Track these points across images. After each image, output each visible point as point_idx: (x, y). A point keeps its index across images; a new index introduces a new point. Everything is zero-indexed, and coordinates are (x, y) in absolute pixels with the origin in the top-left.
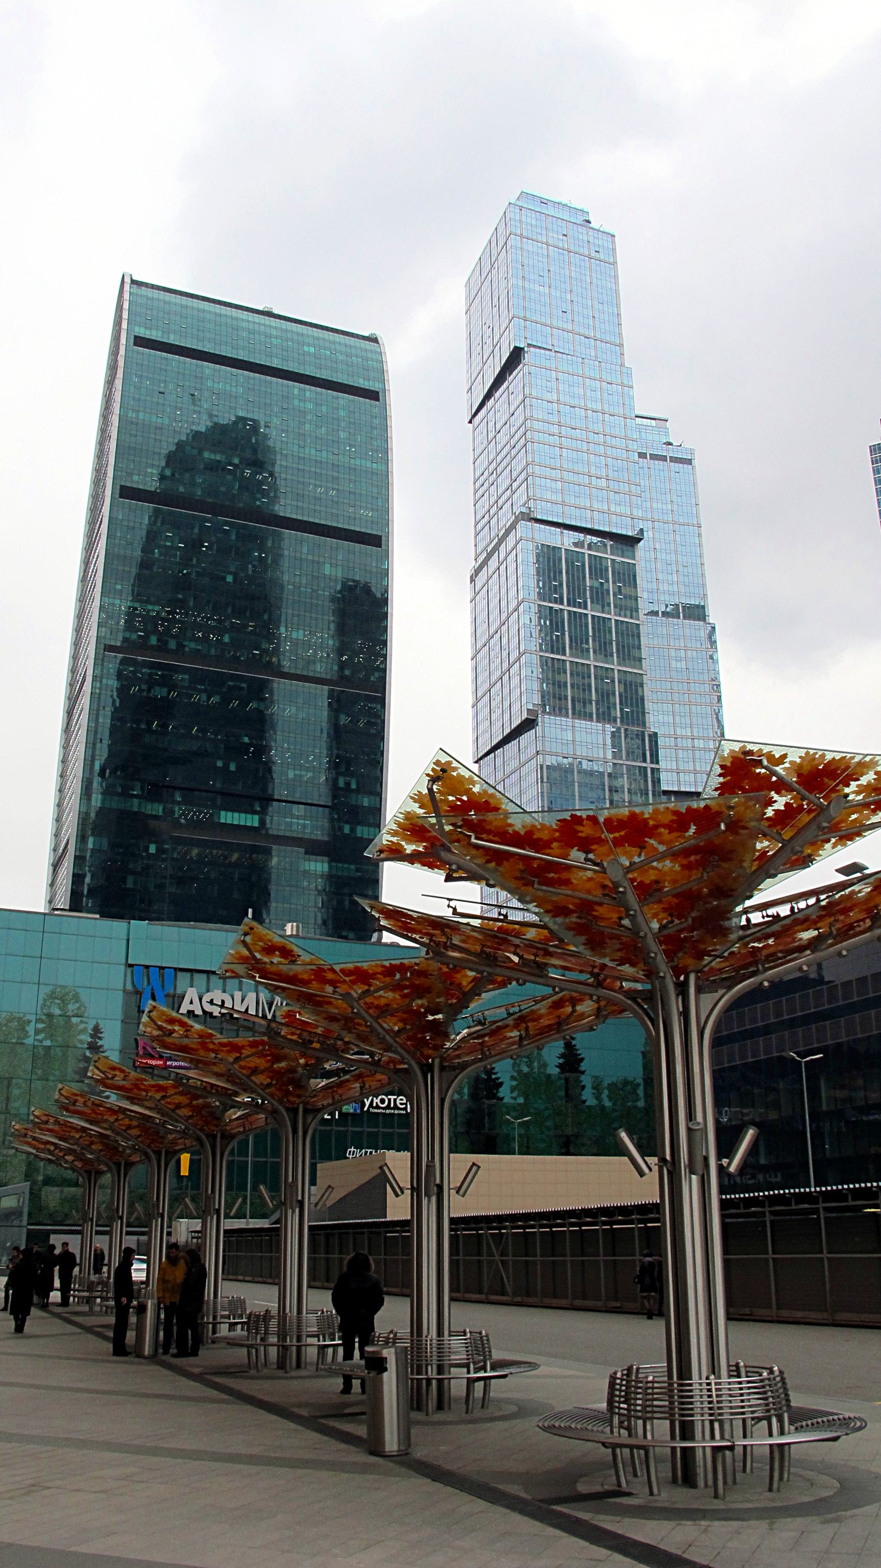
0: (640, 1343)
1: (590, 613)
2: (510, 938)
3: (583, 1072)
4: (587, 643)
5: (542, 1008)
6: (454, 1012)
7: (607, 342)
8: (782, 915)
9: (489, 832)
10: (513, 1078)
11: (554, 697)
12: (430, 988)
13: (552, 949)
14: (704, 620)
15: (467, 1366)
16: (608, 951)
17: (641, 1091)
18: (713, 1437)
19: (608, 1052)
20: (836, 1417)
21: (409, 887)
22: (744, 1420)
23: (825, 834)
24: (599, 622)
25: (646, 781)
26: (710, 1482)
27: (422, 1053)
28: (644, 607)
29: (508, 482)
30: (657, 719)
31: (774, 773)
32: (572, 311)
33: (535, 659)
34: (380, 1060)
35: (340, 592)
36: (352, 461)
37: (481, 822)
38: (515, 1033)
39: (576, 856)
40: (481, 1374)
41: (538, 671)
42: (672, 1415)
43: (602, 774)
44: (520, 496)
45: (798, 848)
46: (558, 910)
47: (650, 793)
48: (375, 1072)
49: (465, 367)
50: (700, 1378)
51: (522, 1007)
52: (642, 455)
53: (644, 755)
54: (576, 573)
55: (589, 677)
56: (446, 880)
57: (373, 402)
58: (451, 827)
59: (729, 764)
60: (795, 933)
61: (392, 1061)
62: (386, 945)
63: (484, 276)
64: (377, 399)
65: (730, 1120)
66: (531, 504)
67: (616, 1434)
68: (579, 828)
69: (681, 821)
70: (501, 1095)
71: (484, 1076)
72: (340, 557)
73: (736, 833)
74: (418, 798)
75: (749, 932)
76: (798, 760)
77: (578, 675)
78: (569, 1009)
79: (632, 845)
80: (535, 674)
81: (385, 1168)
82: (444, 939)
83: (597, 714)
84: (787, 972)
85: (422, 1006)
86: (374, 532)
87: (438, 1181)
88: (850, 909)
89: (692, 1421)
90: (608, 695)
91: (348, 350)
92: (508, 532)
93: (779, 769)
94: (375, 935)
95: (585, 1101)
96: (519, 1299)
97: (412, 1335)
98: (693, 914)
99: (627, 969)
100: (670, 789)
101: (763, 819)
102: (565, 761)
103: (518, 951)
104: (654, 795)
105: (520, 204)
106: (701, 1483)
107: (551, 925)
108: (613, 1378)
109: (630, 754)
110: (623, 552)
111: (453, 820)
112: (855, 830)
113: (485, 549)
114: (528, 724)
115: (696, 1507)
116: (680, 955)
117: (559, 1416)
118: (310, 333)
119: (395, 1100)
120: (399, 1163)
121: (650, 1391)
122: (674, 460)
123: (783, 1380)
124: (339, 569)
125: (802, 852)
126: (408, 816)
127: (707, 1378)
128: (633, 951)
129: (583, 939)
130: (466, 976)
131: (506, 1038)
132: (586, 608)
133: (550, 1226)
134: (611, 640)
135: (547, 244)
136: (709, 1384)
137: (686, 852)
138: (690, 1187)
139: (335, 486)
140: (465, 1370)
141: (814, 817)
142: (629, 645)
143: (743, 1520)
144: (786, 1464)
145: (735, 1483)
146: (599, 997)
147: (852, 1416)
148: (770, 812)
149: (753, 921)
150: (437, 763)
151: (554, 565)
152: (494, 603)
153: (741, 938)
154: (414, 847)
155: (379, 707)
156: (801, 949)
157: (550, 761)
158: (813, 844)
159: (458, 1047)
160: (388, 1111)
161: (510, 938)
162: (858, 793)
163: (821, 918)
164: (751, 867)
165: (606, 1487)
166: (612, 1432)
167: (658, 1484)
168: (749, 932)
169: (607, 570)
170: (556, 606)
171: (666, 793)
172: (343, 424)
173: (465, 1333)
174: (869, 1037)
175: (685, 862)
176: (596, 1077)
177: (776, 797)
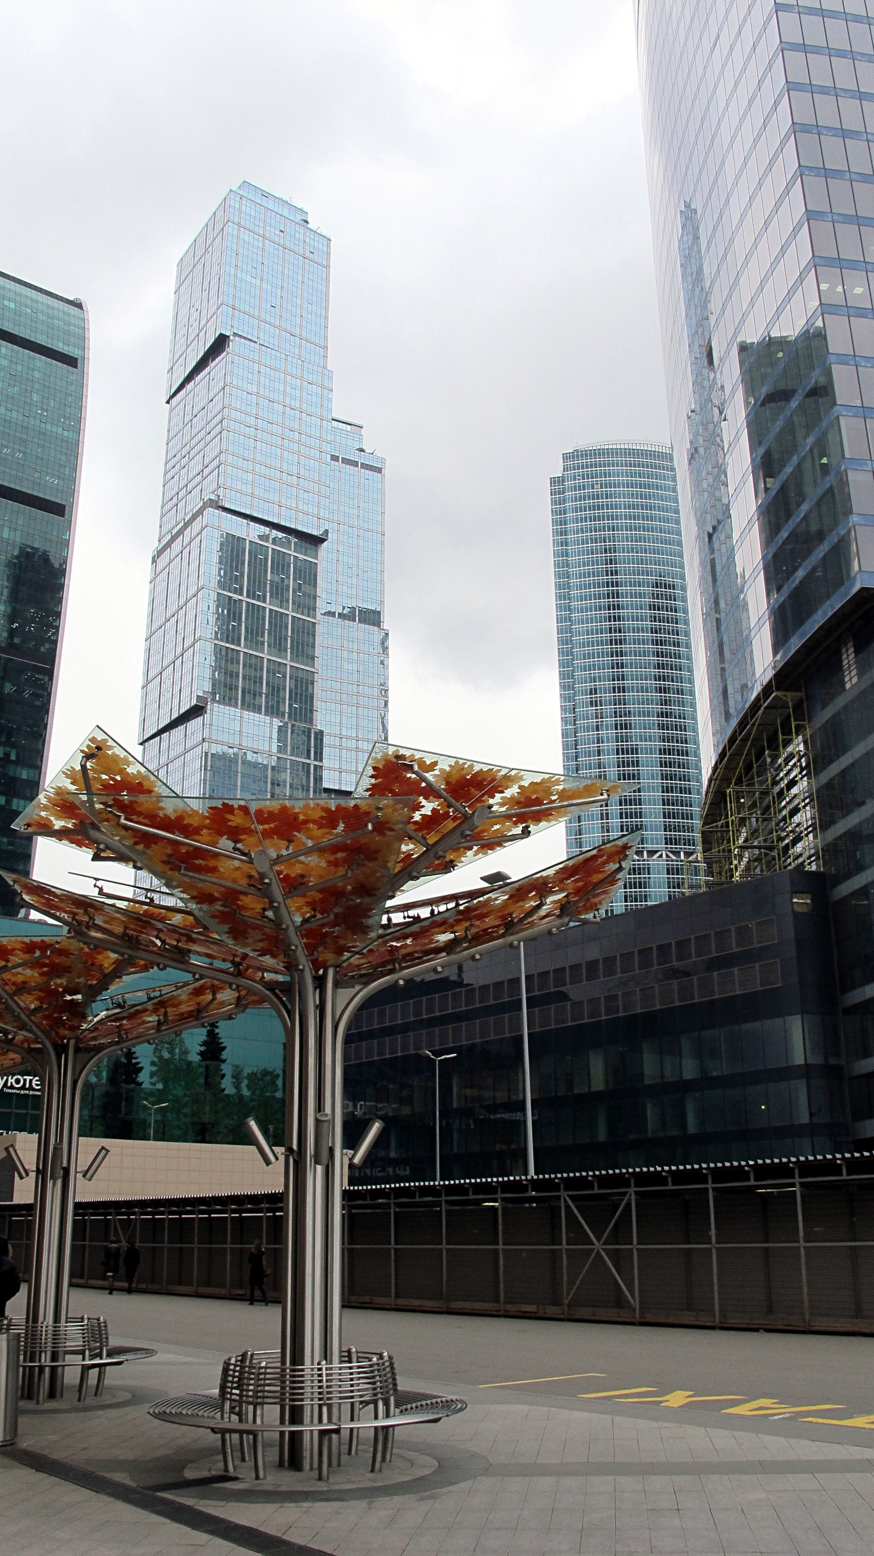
0: (255, 1329)
1: (268, 607)
2: (153, 922)
3: (224, 1061)
4: (263, 636)
5: (183, 994)
6: (92, 994)
7: (312, 341)
8: (422, 917)
9: (139, 814)
10: (153, 1063)
11: (225, 686)
12: (70, 967)
13: (194, 936)
14: (379, 625)
15: (82, 1352)
16: (250, 941)
17: (279, 1082)
18: (320, 1421)
19: (250, 1041)
20: (439, 1400)
21: (60, 865)
22: (352, 1404)
23: (467, 841)
24: (276, 617)
25: (308, 777)
26: (316, 1465)
27: (57, 1033)
28: (322, 606)
29: (200, 467)
30: (324, 719)
31: (423, 779)
32: (281, 307)
33: (210, 647)
34: (13, 1038)
35: (17, 557)
36: (43, 425)
37: (132, 803)
38: (153, 1018)
39: (225, 844)
40: (97, 1361)
41: (211, 660)
42: (283, 1400)
43: (266, 766)
44: (210, 484)
45: (441, 853)
46: (203, 898)
47: (312, 789)
48: (8, 1051)
49: (168, 346)
50: (312, 1364)
51: (163, 993)
52: (334, 458)
53: (309, 751)
54: (258, 565)
55: (262, 669)
56: (93, 859)
57: (70, 368)
58: (102, 806)
59: (381, 767)
60: (433, 934)
61: (26, 1040)
62: (33, 922)
63: (197, 259)
64: (75, 366)
65: (365, 1114)
66: (221, 492)
67: (226, 1420)
68: (229, 817)
69: (330, 819)
70: (140, 1079)
71: (123, 1060)
72: (20, 522)
73: (382, 833)
74: (70, 774)
75: (390, 931)
76: (448, 769)
77: (250, 666)
78: (209, 997)
79: (281, 837)
80: (208, 662)
81: (11, 1149)
82: (86, 919)
83: (266, 707)
84: (418, 973)
85: (61, 985)
86: (59, 501)
87: (65, 1164)
88: (486, 915)
89: (302, 1406)
90: (278, 689)
91: (51, 311)
92: (194, 517)
93: (429, 776)
94: (23, 912)
95: (224, 1090)
96: (144, 1286)
97: (27, 1322)
98: (337, 910)
99: (268, 960)
100: (332, 787)
101: (409, 823)
102: (231, 751)
103: (161, 935)
104: (315, 792)
105: (241, 192)
106: (307, 1466)
107: (196, 913)
108: (227, 1364)
109: (295, 750)
110: (306, 550)
111: (104, 799)
112: (497, 840)
113: (170, 531)
114: (196, 711)
115: (299, 1489)
116: (320, 949)
117: (174, 1402)
118: (29, 294)
119: (31, 1081)
120: (26, 1146)
121: (262, 1377)
122: (365, 466)
123: (392, 1365)
124: (18, 533)
125: (444, 857)
126: (59, 791)
127: (319, 1364)
128: (276, 944)
129: (226, 928)
130: (108, 957)
131: (144, 1022)
132: (264, 601)
133: (180, 1213)
134: (286, 636)
135: (264, 237)
136: (320, 1369)
137: (335, 849)
138: (315, 1178)
139: (23, 449)
140: (81, 1357)
141: (459, 825)
142: (304, 643)
143: (343, 1500)
144: (390, 1446)
145: (339, 1465)
146: (238, 986)
147: (454, 1398)
148: (417, 817)
149: (394, 921)
150: (93, 740)
151: (238, 556)
152: (174, 586)
153: (380, 937)
154: (63, 823)
155: (46, 678)
156: (438, 951)
157: (215, 749)
158: (456, 850)
159: (95, 1029)
160: (22, 1092)
161: (153, 922)
162: (502, 805)
163: (458, 922)
164: (394, 869)
165: (214, 1473)
166: (222, 1418)
167: (264, 1469)
168: (390, 931)
169: (289, 567)
170: (236, 597)
171: (327, 790)
172: (37, 386)
173: (82, 1319)
174: (502, 1039)
175: (332, 858)
176: (237, 1066)
177: (424, 803)
